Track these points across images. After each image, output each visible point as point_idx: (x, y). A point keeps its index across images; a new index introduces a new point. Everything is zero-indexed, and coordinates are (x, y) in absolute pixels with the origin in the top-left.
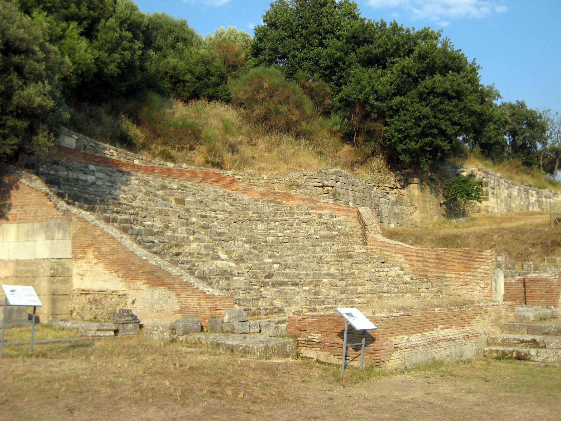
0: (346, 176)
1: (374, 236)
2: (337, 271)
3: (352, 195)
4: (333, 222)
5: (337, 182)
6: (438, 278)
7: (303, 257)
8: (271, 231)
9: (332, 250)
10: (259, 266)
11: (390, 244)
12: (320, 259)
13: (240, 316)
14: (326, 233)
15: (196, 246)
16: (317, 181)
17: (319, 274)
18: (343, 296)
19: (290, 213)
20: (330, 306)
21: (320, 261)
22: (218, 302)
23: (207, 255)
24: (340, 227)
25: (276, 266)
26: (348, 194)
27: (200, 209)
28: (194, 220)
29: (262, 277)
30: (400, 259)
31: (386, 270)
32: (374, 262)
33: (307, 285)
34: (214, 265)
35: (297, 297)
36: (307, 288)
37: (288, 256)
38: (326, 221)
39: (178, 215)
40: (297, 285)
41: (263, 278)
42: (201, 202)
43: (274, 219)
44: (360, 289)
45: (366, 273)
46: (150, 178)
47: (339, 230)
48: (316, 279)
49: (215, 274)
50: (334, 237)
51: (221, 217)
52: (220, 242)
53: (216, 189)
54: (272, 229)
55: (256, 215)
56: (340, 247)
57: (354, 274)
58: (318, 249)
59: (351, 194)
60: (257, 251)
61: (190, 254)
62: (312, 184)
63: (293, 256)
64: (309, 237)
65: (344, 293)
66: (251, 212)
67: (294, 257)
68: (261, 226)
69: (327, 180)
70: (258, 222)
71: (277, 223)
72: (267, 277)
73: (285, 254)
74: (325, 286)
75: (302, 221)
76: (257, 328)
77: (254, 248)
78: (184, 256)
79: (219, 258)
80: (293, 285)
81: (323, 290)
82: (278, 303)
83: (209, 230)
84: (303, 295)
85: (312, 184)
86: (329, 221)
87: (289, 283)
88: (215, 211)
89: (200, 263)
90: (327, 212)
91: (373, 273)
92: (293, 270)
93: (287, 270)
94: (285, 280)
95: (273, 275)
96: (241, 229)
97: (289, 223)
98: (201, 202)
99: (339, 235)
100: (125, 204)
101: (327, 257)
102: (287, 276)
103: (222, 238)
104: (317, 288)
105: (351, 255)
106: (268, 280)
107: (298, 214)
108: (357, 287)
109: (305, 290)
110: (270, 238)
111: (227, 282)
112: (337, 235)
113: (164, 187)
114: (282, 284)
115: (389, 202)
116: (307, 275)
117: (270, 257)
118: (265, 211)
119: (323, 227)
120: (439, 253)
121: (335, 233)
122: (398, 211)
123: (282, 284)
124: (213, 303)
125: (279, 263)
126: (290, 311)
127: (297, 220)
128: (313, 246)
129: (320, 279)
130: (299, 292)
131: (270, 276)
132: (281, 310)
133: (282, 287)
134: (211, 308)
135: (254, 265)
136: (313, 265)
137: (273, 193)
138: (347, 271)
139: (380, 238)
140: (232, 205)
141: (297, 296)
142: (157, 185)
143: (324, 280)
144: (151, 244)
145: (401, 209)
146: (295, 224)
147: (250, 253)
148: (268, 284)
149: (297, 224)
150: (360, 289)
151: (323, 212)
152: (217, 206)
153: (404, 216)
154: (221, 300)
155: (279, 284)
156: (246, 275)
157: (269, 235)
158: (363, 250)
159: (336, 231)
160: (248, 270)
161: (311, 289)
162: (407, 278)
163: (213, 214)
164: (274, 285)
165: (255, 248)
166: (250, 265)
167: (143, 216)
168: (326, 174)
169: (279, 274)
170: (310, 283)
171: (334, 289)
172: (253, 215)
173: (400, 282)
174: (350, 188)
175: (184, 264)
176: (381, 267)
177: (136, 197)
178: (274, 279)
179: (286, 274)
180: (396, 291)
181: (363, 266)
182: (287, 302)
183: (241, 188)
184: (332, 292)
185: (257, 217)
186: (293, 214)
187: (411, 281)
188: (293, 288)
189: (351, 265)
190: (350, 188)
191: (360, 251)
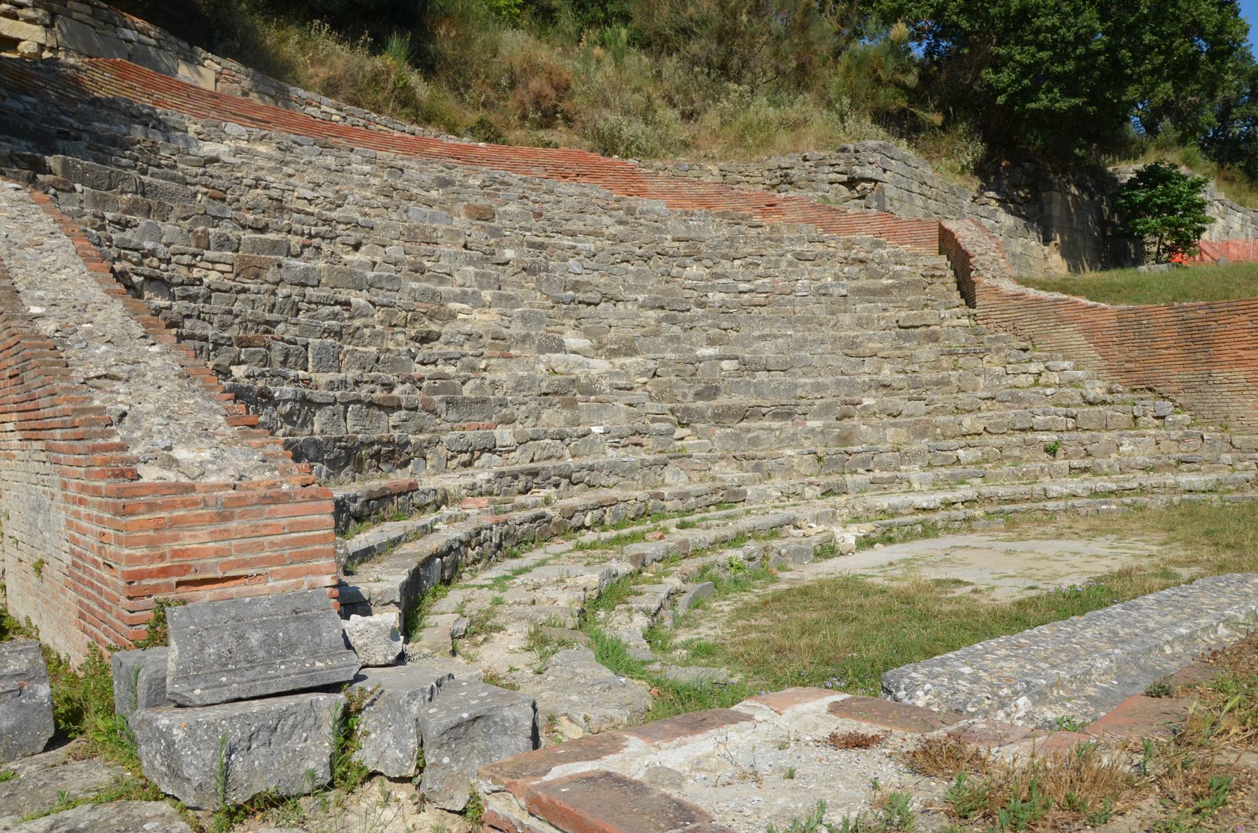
0: (905, 161)
1: (994, 282)
2: (902, 376)
3: (921, 204)
4: (882, 257)
5: (885, 171)
6: (1188, 387)
7: (806, 340)
8: (721, 281)
9: (883, 323)
10: (680, 367)
11: (1039, 300)
12: (853, 344)
13: (291, 646)
14: (863, 282)
15: (497, 317)
16: (837, 169)
17: (852, 384)
18: (924, 443)
19: (771, 240)
20: (886, 475)
21: (851, 348)
22: (203, 533)
23: (525, 339)
24: (898, 268)
25: (726, 365)
26: (912, 199)
27: (530, 230)
28: (509, 254)
29: (685, 395)
30: (1073, 336)
31: (1034, 368)
32: (999, 350)
33: (817, 416)
34: (542, 367)
35: (789, 452)
36: (812, 424)
37: (763, 338)
38: (862, 255)
39: (462, 241)
40: (789, 415)
41: (690, 398)
42: (538, 215)
43: (732, 252)
44: (968, 422)
45: (981, 380)
46: (412, 164)
47: (895, 275)
48: (843, 397)
49: (536, 391)
50: (887, 291)
51: (589, 245)
52: (572, 305)
53: (587, 190)
54: (724, 276)
55: (683, 244)
56: (903, 314)
57: (948, 383)
58: (846, 319)
59: (919, 201)
60: (676, 329)
61: (469, 336)
62: (824, 177)
63: (776, 337)
64: (823, 292)
65: (922, 434)
66: (669, 237)
67: (780, 340)
68: (694, 269)
69: (861, 165)
70: (688, 261)
71: (737, 262)
72: (699, 395)
73: (757, 333)
74: (868, 413)
75: (800, 257)
76: (399, 736)
77: (666, 319)
78: (448, 343)
79: (560, 348)
80: (776, 416)
81: (863, 428)
82: (729, 474)
83: (543, 274)
84: (807, 443)
85: (824, 177)
86: (871, 256)
87: (764, 410)
88: (573, 235)
89: (493, 361)
90: (864, 236)
91: (999, 377)
92: (779, 376)
93: (762, 376)
94: (754, 402)
95: (717, 389)
96: (638, 275)
97: (770, 262)
98: (538, 215)
99: (899, 287)
100: (299, 211)
101: (870, 339)
102: (759, 391)
103: (581, 296)
104: (846, 422)
105: (934, 332)
106: (700, 403)
107: (791, 240)
108: (960, 417)
109: (813, 430)
110: (715, 297)
111: (567, 413)
112: (893, 286)
113: (444, 183)
114: (745, 414)
115: (1000, 228)
116: (818, 387)
117: (712, 342)
118: (706, 236)
119: (856, 269)
120: (1192, 315)
121: (886, 281)
122: (1019, 250)
123: (745, 414)
124: (151, 543)
125: (737, 358)
126: (764, 496)
127: (789, 256)
128: (833, 314)
129: (856, 399)
130: (793, 437)
131: (710, 392)
132: (732, 498)
133: (744, 424)
134: (141, 575)
135: (665, 364)
136: (838, 361)
137: (730, 198)
138: (926, 376)
139: (1008, 287)
140: (621, 223)
141: (788, 446)
142: (425, 178)
143: (867, 401)
144: (338, 308)
145: (1025, 246)
146: (783, 265)
147: (656, 333)
148: (701, 416)
149: (790, 264)
150: (968, 422)
151: (857, 237)
152: (581, 223)
153: (1032, 262)
154: (224, 517)
155: (734, 416)
156: (639, 391)
157: (713, 288)
158: (965, 321)
159: (891, 278)
160: (644, 379)
161: (829, 426)
162: (1096, 390)
163: (567, 241)
164: (720, 417)
165: (673, 321)
166: (651, 365)
167: (352, 241)
168: (857, 151)
169: (735, 387)
170: (826, 410)
171: (895, 425)
172: (676, 244)
173: (1079, 399)
174: (915, 188)
175: (435, 363)
176: (1019, 362)
177: (346, 197)
178: (722, 400)
179: (755, 385)
180: (1070, 426)
181: (972, 361)
182: (757, 468)
183: (650, 187)
184: (890, 432)
185: (685, 247)
186: (780, 240)
187: (1109, 398)
188: (776, 424)
189: (938, 360)
190: (915, 188)
191: (955, 322)
